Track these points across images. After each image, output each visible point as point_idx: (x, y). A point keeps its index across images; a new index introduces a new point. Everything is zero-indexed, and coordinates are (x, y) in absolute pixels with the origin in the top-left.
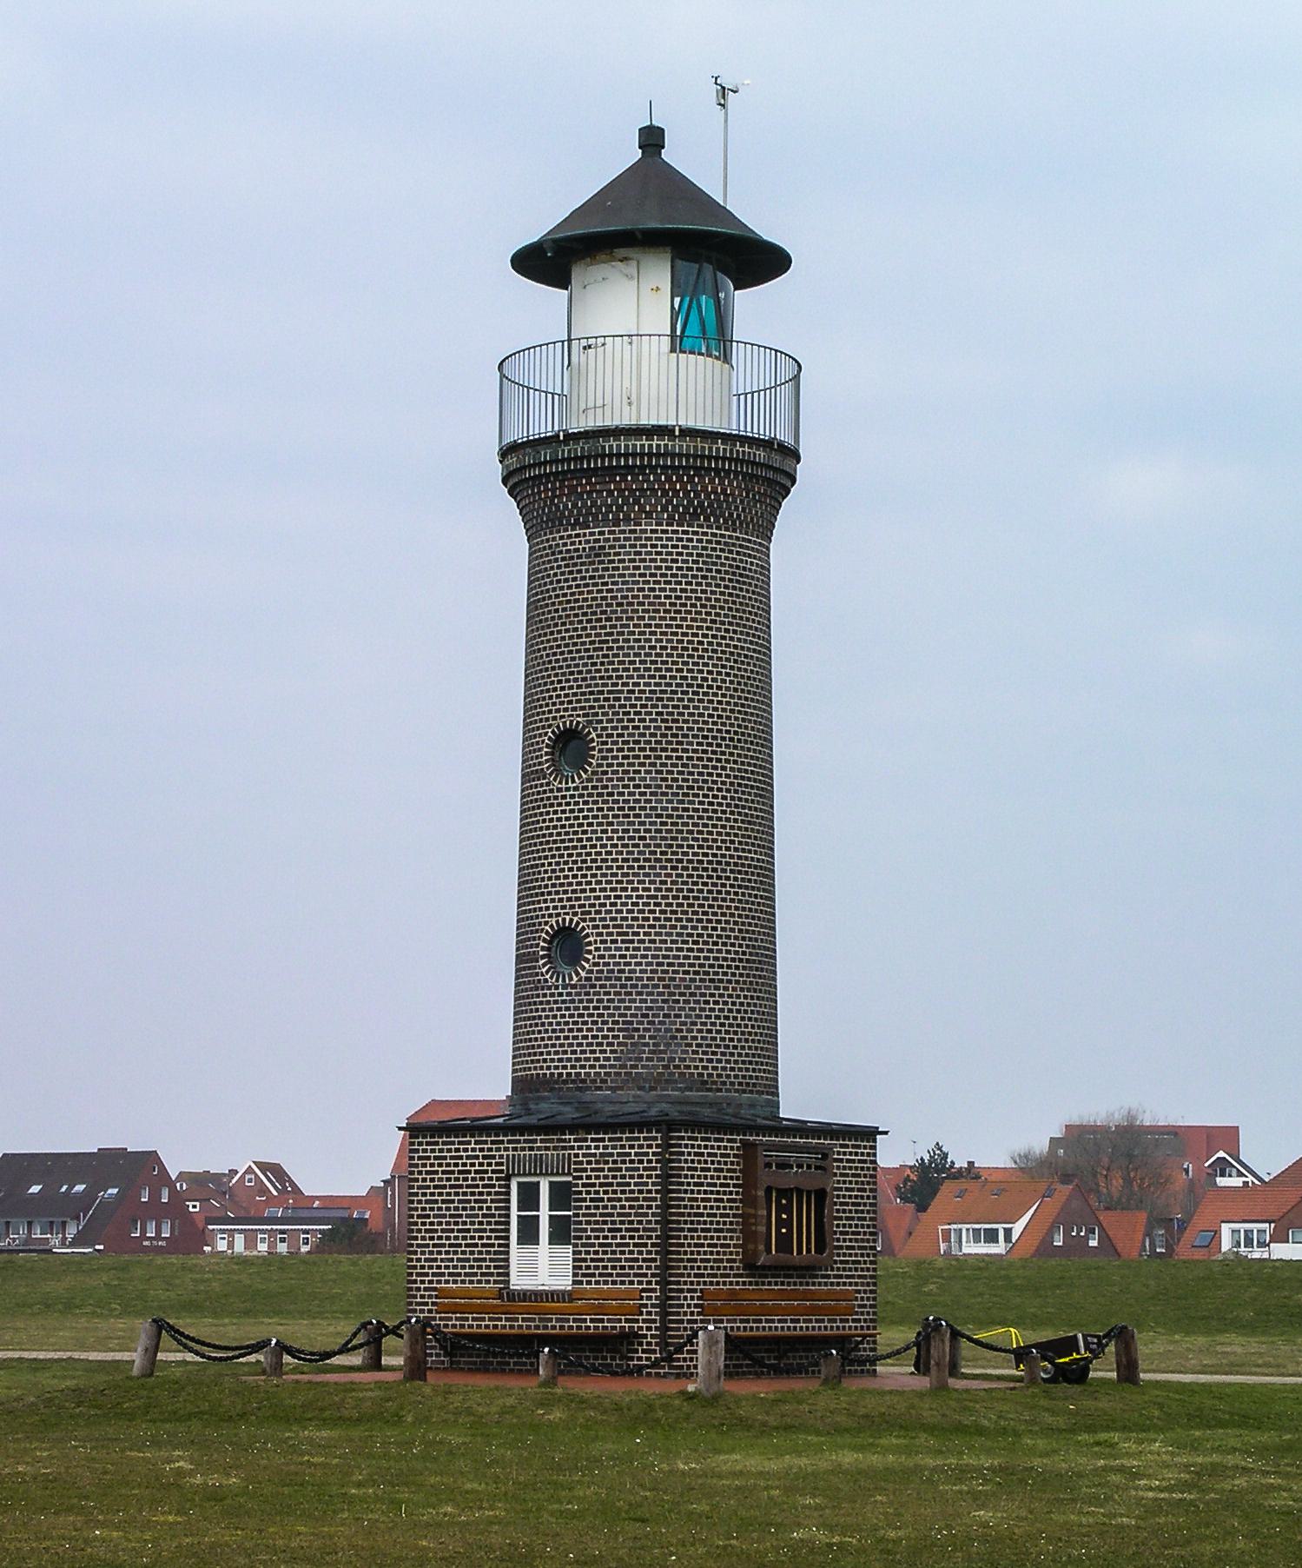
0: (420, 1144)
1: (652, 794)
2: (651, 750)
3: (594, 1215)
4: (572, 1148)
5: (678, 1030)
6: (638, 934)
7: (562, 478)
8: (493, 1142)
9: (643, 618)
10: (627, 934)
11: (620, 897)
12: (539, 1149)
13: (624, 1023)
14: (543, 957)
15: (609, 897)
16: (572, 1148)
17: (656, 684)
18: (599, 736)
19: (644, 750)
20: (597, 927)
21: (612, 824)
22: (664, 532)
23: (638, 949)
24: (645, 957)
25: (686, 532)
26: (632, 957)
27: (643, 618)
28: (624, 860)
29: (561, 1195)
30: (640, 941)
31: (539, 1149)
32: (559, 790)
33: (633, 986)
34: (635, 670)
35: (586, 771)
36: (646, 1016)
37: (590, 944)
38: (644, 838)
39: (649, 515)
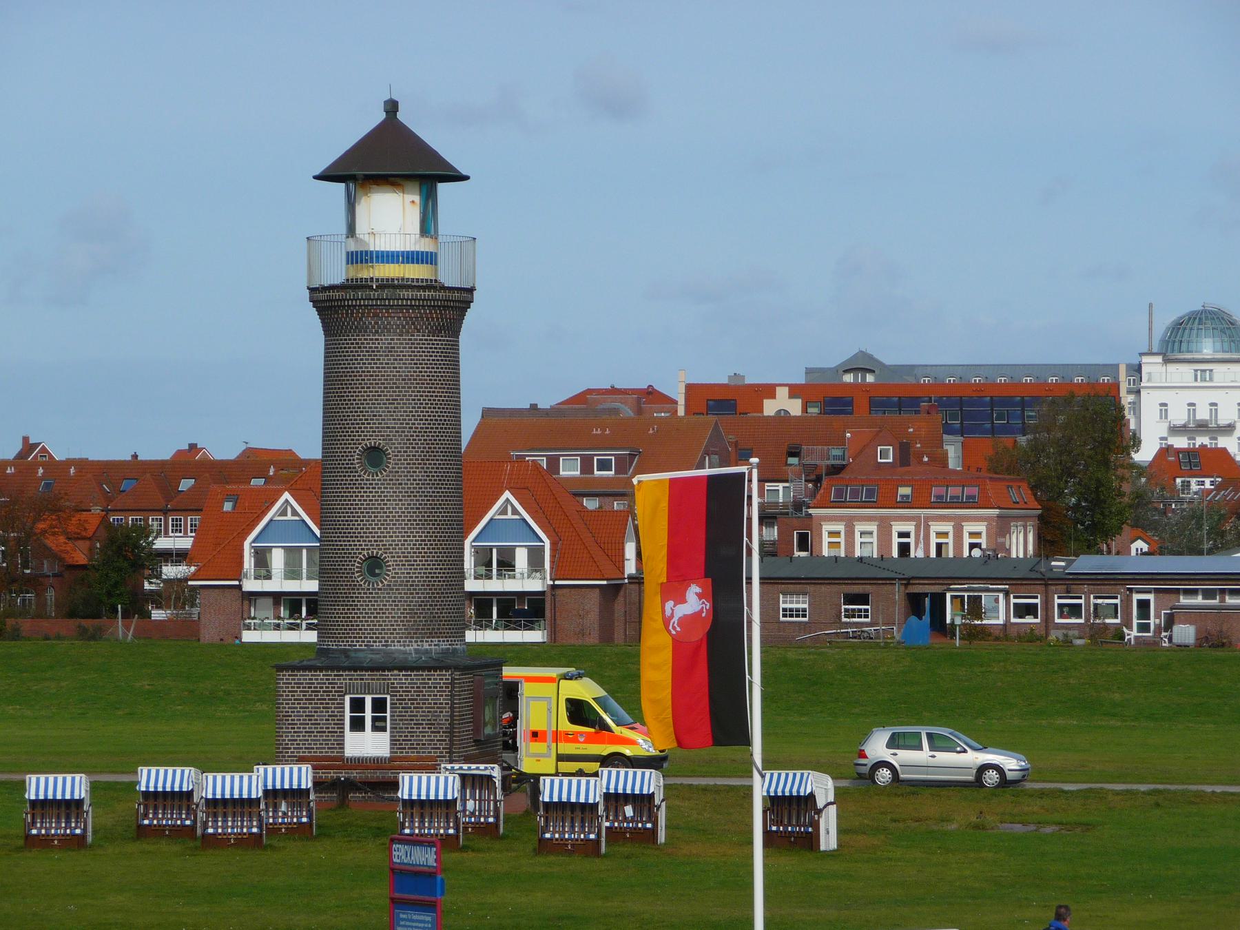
29: (379, 705)
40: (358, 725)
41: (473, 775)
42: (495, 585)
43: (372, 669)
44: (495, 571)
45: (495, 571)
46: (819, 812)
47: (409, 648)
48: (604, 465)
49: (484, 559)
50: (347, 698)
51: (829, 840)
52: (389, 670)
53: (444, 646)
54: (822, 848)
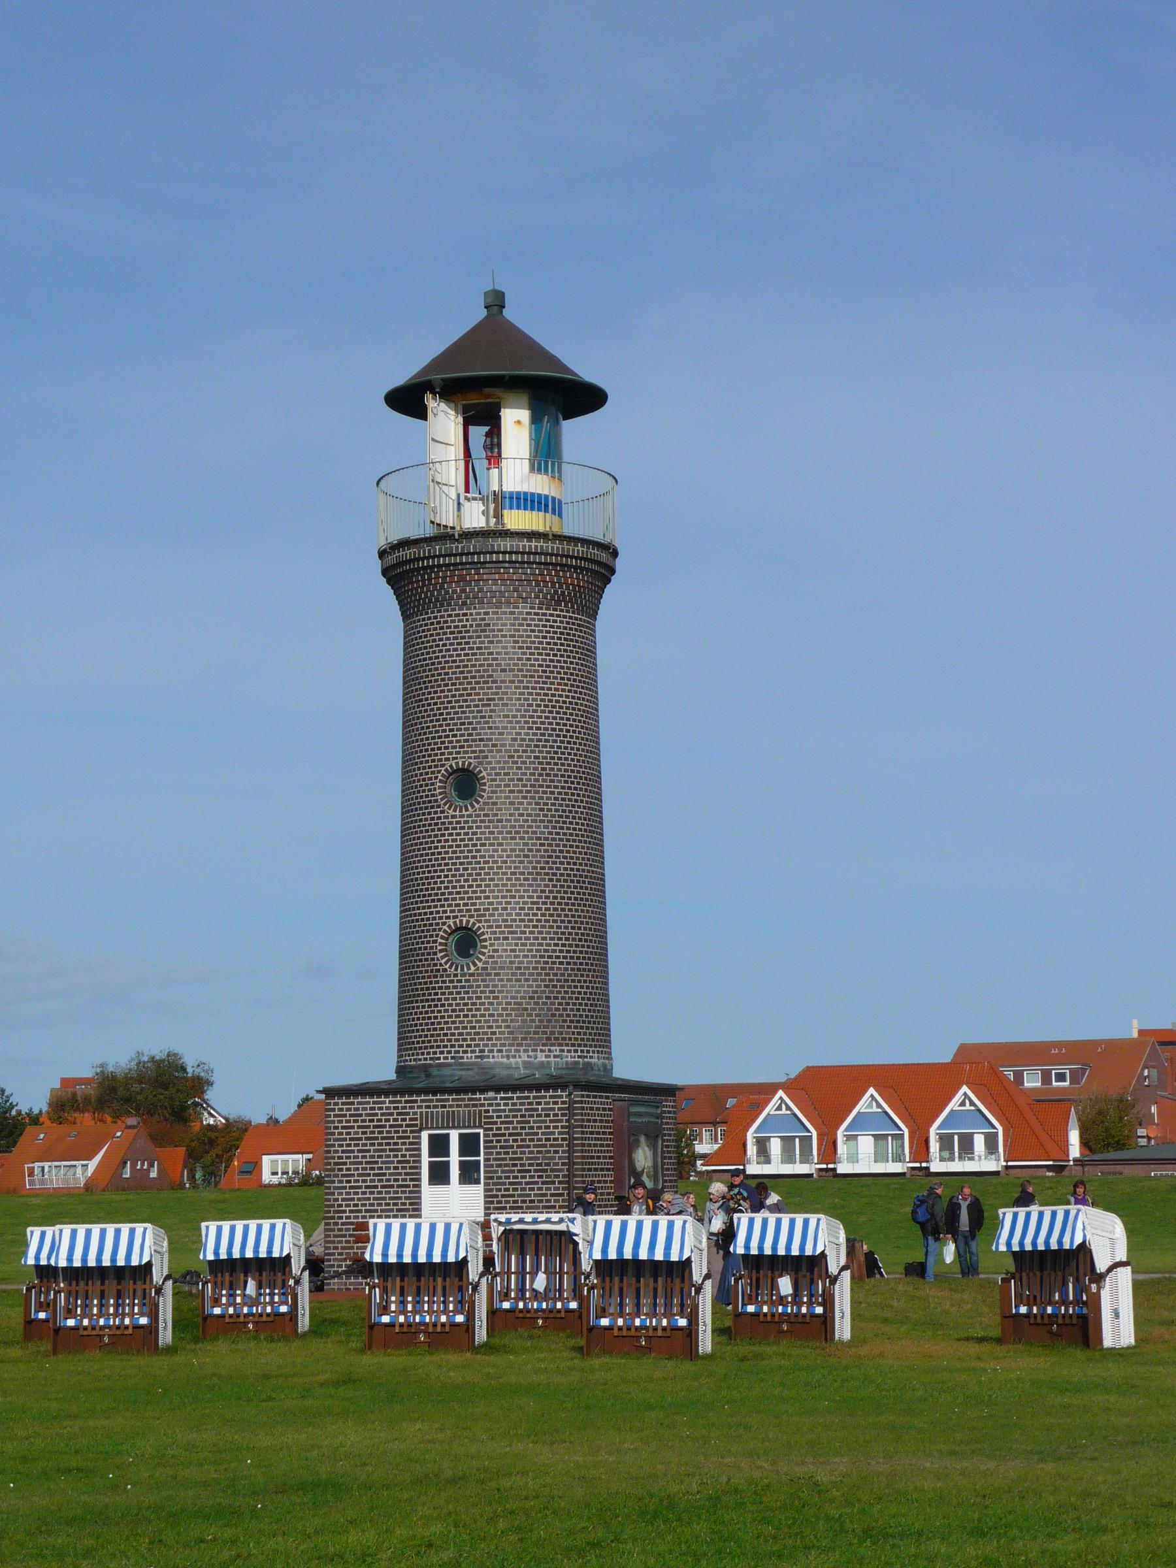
0: (337, 1104)
1: (533, 821)
2: (532, 786)
3: (505, 1159)
4: (483, 1105)
5: (557, 1009)
6: (525, 932)
7: (420, 573)
8: (406, 1102)
9: (522, 682)
10: (515, 932)
11: (509, 903)
12: (451, 1106)
13: (515, 1003)
14: (441, 951)
15: (501, 903)
16: (483, 1105)
17: (534, 734)
18: (488, 775)
19: (526, 786)
20: (491, 927)
21: (501, 844)
22: (536, 614)
23: (525, 945)
24: (531, 951)
25: (551, 615)
26: (520, 951)
27: (522, 682)
28: (512, 874)
29: (469, 1145)
30: (527, 938)
31: (451, 1106)
32: (453, 817)
33: (521, 974)
34: (517, 722)
35: (478, 802)
36: (532, 998)
37: (485, 940)
38: (527, 856)
39: (525, 600)
40: (440, 1175)
41: (537, 1233)
42: (956, 1166)
43: (458, 1091)
44: (957, 1154)
45: (957, 1154)
46: (1099, 1278)
47: (513, 1060)
48: (1061, 1077)
49: (946, 1142)
50: (425, 1135)
51: (1118, 1326)
52: (482, 1091)
53: (569, 1058)
54: (1108, 1342)
